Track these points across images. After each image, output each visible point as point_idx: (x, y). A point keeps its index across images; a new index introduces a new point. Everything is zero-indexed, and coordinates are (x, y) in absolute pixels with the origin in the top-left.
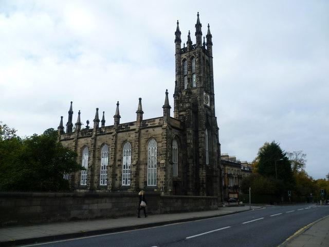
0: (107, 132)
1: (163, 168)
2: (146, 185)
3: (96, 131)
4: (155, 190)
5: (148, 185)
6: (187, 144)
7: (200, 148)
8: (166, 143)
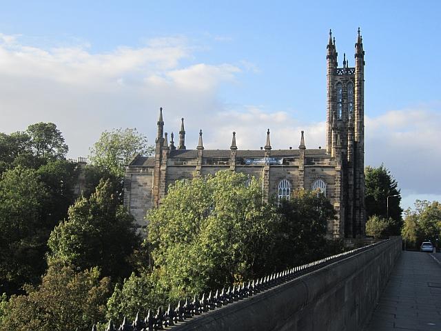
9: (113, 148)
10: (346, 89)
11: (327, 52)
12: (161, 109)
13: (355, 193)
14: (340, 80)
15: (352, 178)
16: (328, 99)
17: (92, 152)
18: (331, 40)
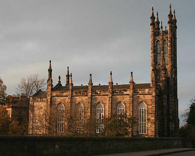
0: (102, 94)
1: (153, 123)
2: (138, 133)
3: (91, 92)
4: (146, 137)
5: (139, 133)
6: (163, 106)
7: (170, 108)
8: (155, 107)
9: (28, 87)
11: (150, 21)
12: (132, 73)
13: (168, 111)
15: (166, 101)
16: (151, 51)
17: (152, 132)
18: (171, 12)
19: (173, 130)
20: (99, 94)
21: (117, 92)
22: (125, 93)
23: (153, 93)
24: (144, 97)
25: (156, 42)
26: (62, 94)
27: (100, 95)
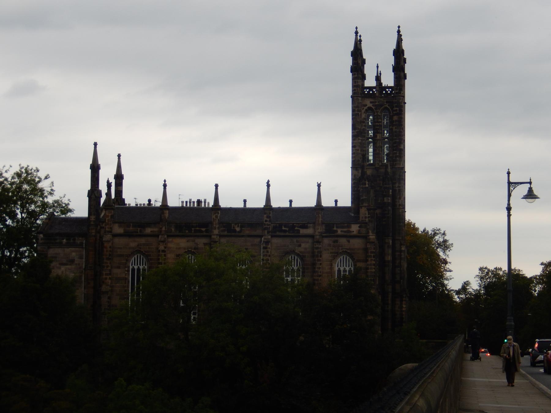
10: (378, 116)
14: (371, 105)
15: (390, 251)
19: (404, 313)
20: (239, 232)
21: (283, 228)
22: (303, 231)
23: (371, 234)
24: (349, 241)
25: (363, 111)
26: (140, 231)
27: (243, 236)
